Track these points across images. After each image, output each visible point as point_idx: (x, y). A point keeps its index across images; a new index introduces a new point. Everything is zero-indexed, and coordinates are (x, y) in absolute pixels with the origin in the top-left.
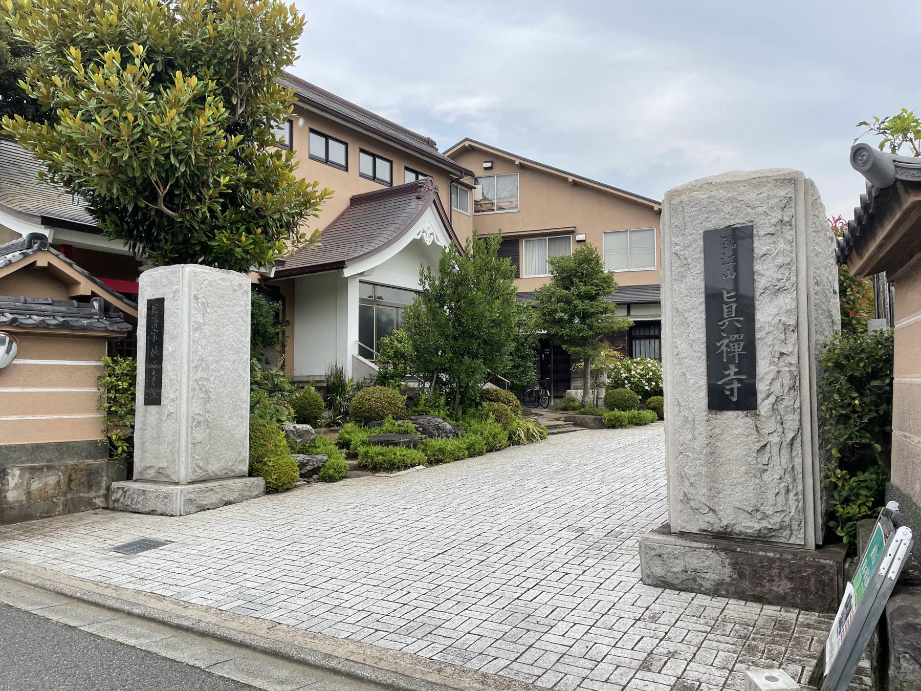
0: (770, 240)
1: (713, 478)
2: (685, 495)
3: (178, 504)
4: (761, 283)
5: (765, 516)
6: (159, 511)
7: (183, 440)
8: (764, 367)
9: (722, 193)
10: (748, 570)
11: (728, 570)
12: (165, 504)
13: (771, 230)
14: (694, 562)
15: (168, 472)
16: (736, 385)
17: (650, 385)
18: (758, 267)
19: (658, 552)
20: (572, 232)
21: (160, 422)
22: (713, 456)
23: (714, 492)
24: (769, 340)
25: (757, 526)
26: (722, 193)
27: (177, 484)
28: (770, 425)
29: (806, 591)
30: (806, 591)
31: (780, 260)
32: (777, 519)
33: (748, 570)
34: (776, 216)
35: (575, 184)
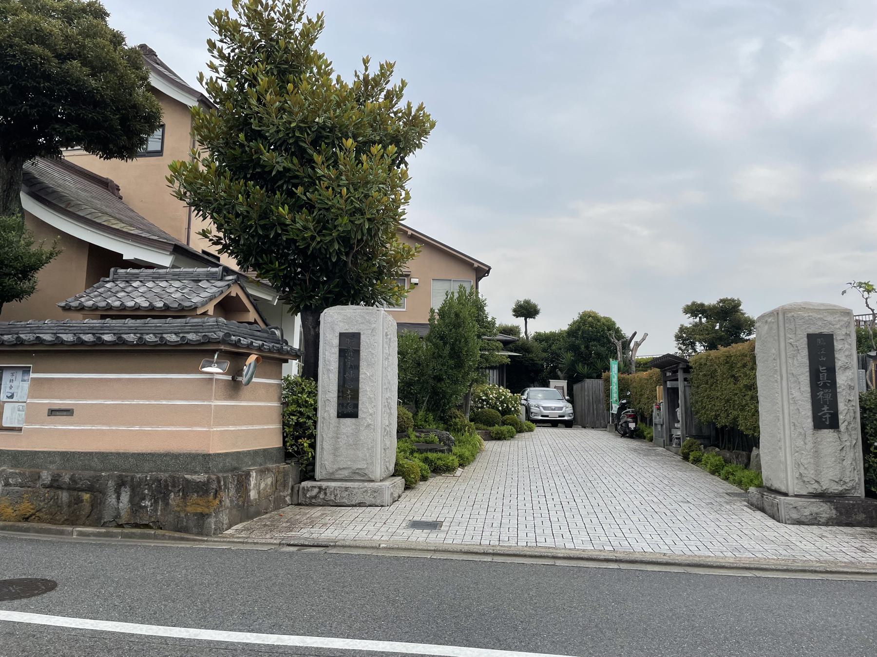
0: (842, 342)
1: (817, 465)
2: (801, 474)
3: (387, 498)
4: (838, 364)
5: (845, 483)
6: (368, 503)
8: (841, 406)
9: (815, 315)
10: (843, 511)
11: (834, 512)
12: (374, 497)
13: (842, 337)
14: (815, 509)
19: (795, 505)
22: (817, 454)
23: (818, 472)
24: (844, 393)
25: (841, 489)
26: (815, 315)
27: (373, 481)
29: (872, 518)
30: (872, 518)
31: (847, 353)
32: (850, 484)
33: (843, 511)
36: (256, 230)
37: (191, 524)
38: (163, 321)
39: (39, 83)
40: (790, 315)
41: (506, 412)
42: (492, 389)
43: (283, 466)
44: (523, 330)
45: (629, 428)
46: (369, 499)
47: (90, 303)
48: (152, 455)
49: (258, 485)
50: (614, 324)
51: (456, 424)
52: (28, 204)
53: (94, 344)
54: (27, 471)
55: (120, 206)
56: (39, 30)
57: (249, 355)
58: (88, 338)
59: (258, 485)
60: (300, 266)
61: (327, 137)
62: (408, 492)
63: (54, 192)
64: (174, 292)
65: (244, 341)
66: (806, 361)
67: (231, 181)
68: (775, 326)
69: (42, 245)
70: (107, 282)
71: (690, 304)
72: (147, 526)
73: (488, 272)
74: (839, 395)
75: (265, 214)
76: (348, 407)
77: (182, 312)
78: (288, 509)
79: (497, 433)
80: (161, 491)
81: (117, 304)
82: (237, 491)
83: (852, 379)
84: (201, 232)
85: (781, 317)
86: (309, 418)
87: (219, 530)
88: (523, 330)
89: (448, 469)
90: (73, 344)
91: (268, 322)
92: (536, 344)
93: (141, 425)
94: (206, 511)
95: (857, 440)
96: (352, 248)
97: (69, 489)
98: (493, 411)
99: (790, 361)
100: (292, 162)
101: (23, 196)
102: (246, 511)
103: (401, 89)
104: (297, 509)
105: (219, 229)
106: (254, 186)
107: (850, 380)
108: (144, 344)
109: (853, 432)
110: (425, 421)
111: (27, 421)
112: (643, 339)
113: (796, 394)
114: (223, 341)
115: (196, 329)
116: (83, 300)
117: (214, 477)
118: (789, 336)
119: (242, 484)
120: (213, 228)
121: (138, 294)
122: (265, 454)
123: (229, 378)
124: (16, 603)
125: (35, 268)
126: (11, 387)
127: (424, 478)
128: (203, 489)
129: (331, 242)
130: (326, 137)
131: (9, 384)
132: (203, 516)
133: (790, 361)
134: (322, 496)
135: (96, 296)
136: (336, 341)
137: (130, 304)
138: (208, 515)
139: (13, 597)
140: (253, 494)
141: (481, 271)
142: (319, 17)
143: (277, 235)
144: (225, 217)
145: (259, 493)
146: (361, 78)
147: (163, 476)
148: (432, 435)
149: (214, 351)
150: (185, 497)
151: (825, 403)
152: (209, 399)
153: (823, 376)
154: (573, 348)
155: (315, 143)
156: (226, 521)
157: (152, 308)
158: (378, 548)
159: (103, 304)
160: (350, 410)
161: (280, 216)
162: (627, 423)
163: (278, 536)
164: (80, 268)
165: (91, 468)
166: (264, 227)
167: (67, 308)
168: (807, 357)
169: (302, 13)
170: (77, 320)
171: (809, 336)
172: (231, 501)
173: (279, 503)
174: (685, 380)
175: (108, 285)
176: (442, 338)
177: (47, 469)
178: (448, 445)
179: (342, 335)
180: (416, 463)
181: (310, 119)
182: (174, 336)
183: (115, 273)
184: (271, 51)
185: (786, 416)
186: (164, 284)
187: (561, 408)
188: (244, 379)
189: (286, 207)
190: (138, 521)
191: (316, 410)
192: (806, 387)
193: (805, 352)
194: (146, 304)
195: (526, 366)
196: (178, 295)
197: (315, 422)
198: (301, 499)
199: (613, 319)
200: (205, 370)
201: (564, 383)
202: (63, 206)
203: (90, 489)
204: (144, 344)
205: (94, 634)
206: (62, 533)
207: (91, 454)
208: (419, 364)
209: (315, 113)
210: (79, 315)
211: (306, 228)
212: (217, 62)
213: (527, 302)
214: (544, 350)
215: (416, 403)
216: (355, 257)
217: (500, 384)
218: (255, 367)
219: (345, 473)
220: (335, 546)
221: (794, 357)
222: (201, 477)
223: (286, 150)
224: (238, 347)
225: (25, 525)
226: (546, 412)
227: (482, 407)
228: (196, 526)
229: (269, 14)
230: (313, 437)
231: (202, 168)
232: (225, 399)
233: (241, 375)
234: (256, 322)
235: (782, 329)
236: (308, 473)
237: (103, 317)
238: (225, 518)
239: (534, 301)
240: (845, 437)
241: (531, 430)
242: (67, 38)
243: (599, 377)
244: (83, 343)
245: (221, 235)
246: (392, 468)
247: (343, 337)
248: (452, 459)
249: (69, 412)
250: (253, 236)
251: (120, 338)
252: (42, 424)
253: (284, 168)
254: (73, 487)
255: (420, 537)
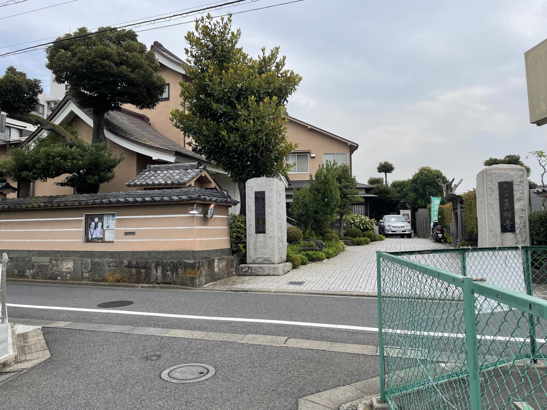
3: (281, 272)
4: (515, 198)
7: (276, 247)
8: (517, 220)
9: (503, 172)
15: (271, 259)
16: (509, 225)
17: (363, 226)
18: (515, 193)
20: (309, 153)
21: (265, 240)
24: (518, 213)
26: (503, 172)
27: (274, 264)
28: (519, 236)
31: (521, 192)
34: (519, 180)
35: (311, 130)
36: (213, 143)
37: (188, 282)
38: (171, 190)
39: (108, 79)
40: (489, 172)
41: (366, 229)
42: (358, 216)
43: (231, 257)
44: (385, 180)
45: (438, 237)
46: (272, 272)
47: (139, 183)
48: (170, 252)
49: (218, 265)
50: (441, 174)
51: (328, 236)
52: (108, 135)
53: (142, 202)
54: (117, 260)
55: (150, 129)
56: (106, 53)
57: (211, 204)
58: (139, 199)
59: (218, 266)
60: (236, 158)
61: (244, 94)
62: (294, 270)
63: (119, 128)
64: (176, 176)
65: (208, 198)
66: (498, 197)
67: (200, 118)
68: (482, 179)
69: (116, 155)
70: (146, 172)
71: (488, 159)
72: (169, 283)
73: (357, 147)
74: (515, 214)
75: (217, 134)
76: (261, 228)
77: (179, 185)
78: (234, 277)
79: (358, 242)
80: (175, 268)
81: (151, 182)
82: (209, 268)
83: (523, 205)
84: (188, 143)
85: (485, 174)
86: (242, 234)
87: (201, 285)
88: (385, 180)
89: (320, 259)
90: (133, 202)
91: (221, 187)
92: (394, 189)
93: (165, 238)
94: (195, 276)
95: (526, 238)
96: (259, 148)
97: (136, 268)
98: (357, 229)
99: (489, 197)
100: (228, 109)
101: (105, 131)
102: (213, 277)
103: (284, 61)
104: (238, 277)
105: (196, 142)
106: (211, 120)
107: (521, 206)
108: (163, 202)
109: (523, 234)
110: (310, 235)
111: (116, 238)
112: (460, 183)
113: (492, 214)
114: (198, 199)
115: (186, 193)
116: (136, 181)
117: (197, 261)
118: (488, 183)
119: (211, 265)
120: (193, 141)
121: (160, 177)
122: (222, 251)
123: (202, 216)
124: (118, 308)
125: (113, 167)
126: (108, 223)
127: (304, 264)
128: (192, 266)
129: (248, 146)
130: (241, 95)
131: (107, 222)
132: (193, 279)
133: (489, 197)
134: (250, 271)
135: (141, 179)
136: (253, 196)
137: (157, 182)
138: (196, 278)
139: (117, 306)
140: (216, 270)
141: (353, 148)
142: (238, 31)
143: (223, 145)
144: (198, 137)
145: (219, 269)
146: (262, 58)
147: (175, 261)
148: (312, 242)
149: (194, 204)
150: (185, 270)
151: (508, 218)
152: (194, 226)
153: (507, 205)
154: (416, 190)
155: (238, 98)
156: (204, 281)
157: (166, 184)
158: (270, 292)
159: (145, 183)
160: (261, 229)
161: (223, 136)
162: (437, 234)
163: (226, 287)
164: (132, 165)
165: (144, 258)
166: (216, 141)
167: (129, 186)
168: (498, 195)
169: (230, 30)
170: (133, 191)
171: (499, 183)
172: (206, 272)
173: (230, 275)
174: (461, 208)
175: (147, 173)
176: (317, 190)
177: (126, 259)
178: (321, 247)
179: (256, 193)
180: (299, 256)
181: (234, 86)
182: (176, 197)
183: (149, 167)
184: (216, 49)
185: (487, 226)
186: (171, 172)
187: (404, 227)
188: (209, 216)
189: (226, 131)
190: (166, 281)
191: (245, 230)
192: (498, 211)
193: (497, 192)
194: (163, 182)
195: (381, 201)
196: (177, 177)
197: (245, 236)
198: (240, 273)
199: (441, 171)
200: (190, 212)
201: (409, 212)
202: (123, 135)
203: (144, 267)
204: (163, 202)
205: (148, 316)
206: (134, 287)
207: (144, 252)
208: (306, 205)
209: (237, 83)
210: (135, 188)
211: (235, 141)
212: (190, 59)
213: (386, 163)
214: (399, 192)
215: (306, 224)
216: (262, 152)
217: (366, 215)
218: (214, 210)
219: (261, 260)
220: (251, 291)
221: (491, 194)
222: (192, 261)
223: (224, 102)
224: (205, 201)
225: (118, 284)
226: (394, 229)
227: (351, 227)
228: (189, 283)
229: (213, 33)
230: (245, 243)
231: (187, 112)
232: (201, 225)
233: (207, 214)
234: (215, 188)
235: (485, 180)
236: (243, 260)
237: (145, 189)
238: (203, 279)
239: (390, 162)
240: (519, 236)
241: (381, 239)
242: (119, 54)
243: (425, 207)
244: (137, 202)
245: (197, 144)
246: (284, 258)
247: (257, 193)
248: (321, 254)
249: (133, 233)
250: (212, 146)
251: (152, 199)
252: (122, 239)
253: (224, 111)
254: (137, 267)
255: (292, 288)
